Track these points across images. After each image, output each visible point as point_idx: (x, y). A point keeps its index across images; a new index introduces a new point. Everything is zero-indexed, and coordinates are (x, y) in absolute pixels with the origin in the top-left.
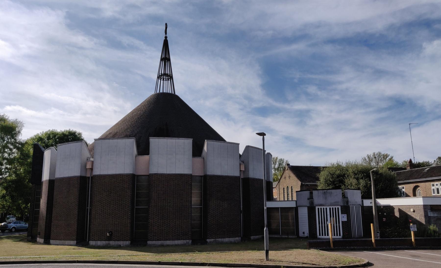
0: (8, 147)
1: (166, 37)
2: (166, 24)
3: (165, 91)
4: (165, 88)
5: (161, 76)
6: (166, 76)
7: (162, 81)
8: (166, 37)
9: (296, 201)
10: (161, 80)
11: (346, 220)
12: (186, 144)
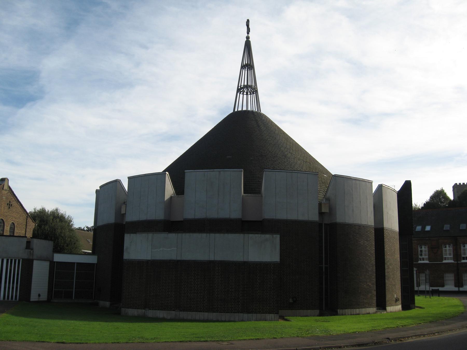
0: (248, 90)
1: (248, 38)
2: (248, 21)
3: (249, 109)
4: (245, 103)
5: (243, 88)
6: (249, 88)
7: (245, 96)
8: (248, 38)
9: (3, 189)
10: (243, 94)
11: (276, 258)
12: (236, 177)
